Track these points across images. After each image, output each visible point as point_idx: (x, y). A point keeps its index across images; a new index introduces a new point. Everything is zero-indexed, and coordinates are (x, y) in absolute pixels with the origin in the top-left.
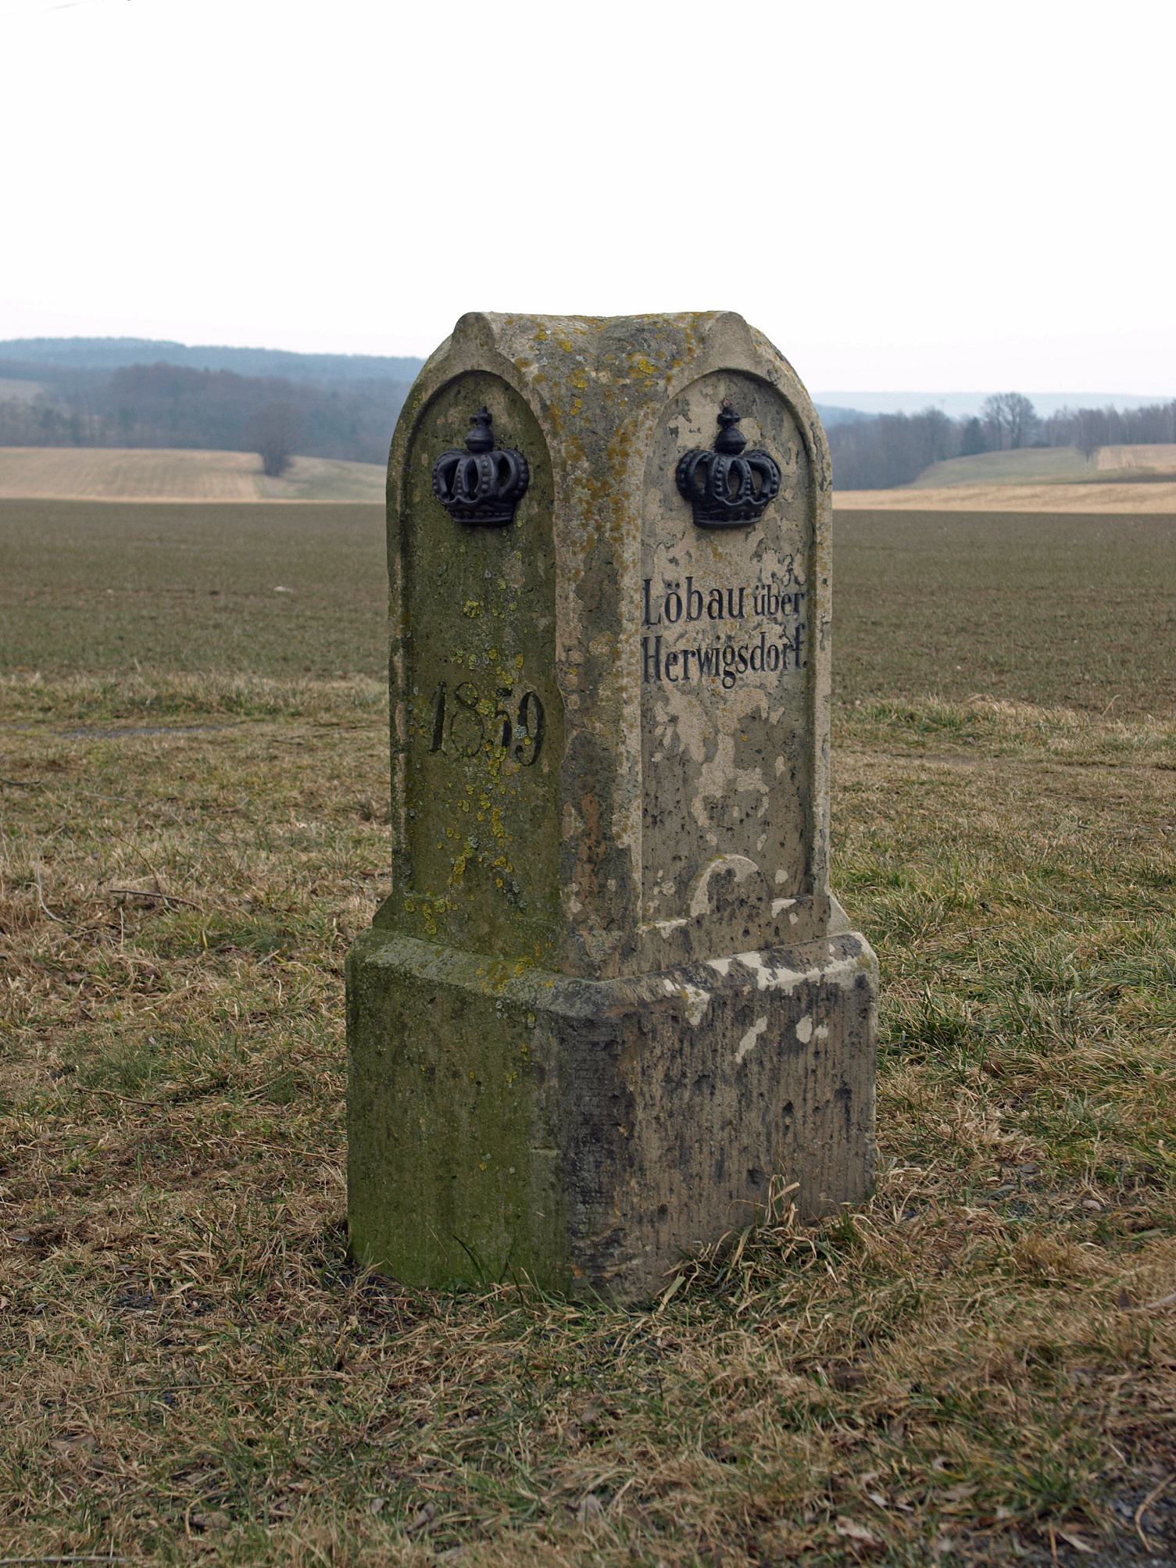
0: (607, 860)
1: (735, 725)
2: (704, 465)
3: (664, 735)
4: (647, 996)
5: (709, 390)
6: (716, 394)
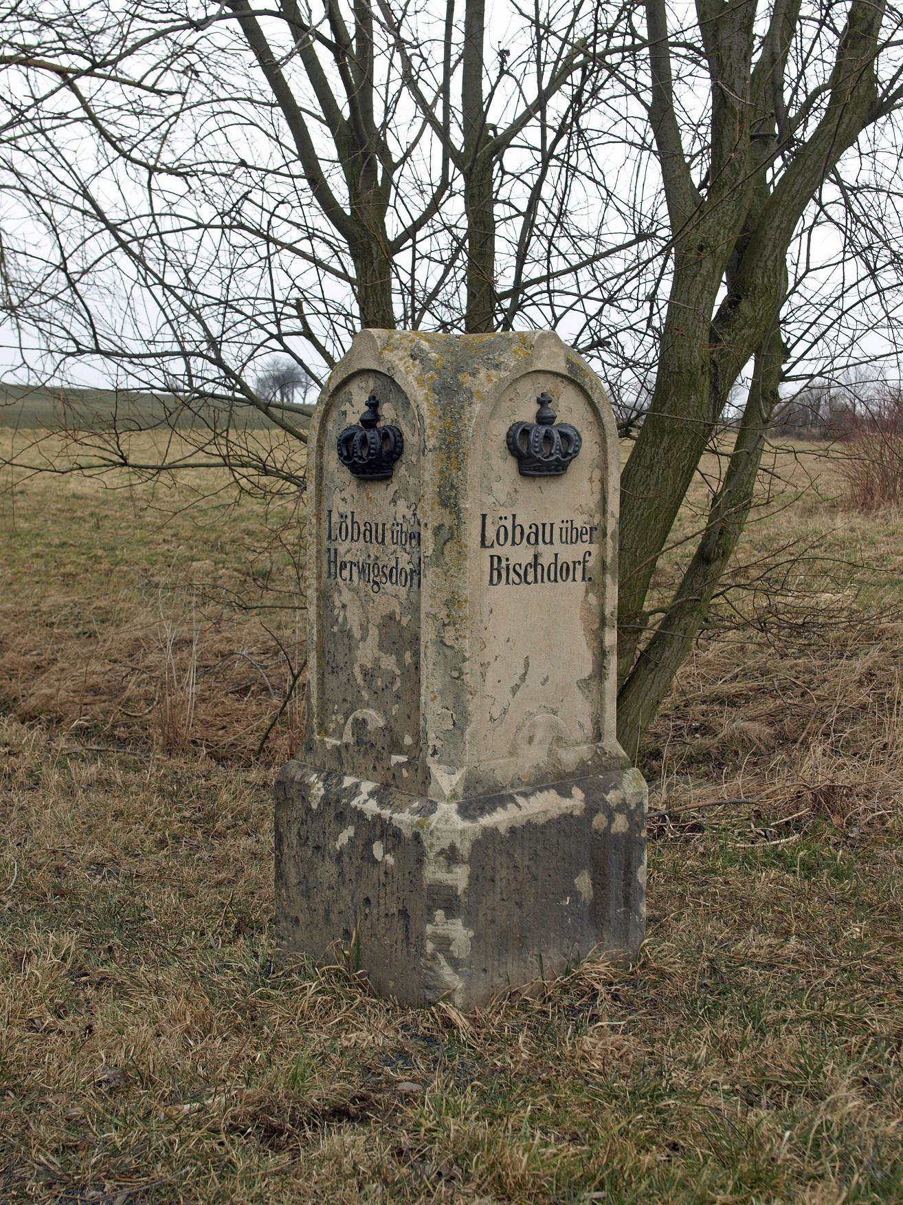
1: (379, 620)
2: (526, 432)
4: (298, 777)
5: (363, 385)
6: (367, 387)
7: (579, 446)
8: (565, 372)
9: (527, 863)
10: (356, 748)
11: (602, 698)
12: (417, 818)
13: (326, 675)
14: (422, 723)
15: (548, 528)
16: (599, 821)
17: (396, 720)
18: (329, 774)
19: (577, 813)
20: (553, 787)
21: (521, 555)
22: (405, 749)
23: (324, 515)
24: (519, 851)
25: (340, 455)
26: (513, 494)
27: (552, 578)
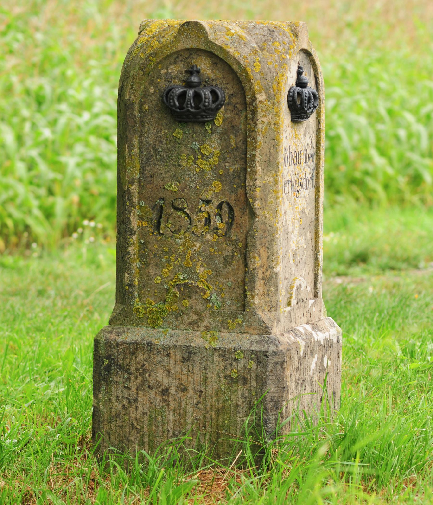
0: (271, 278)
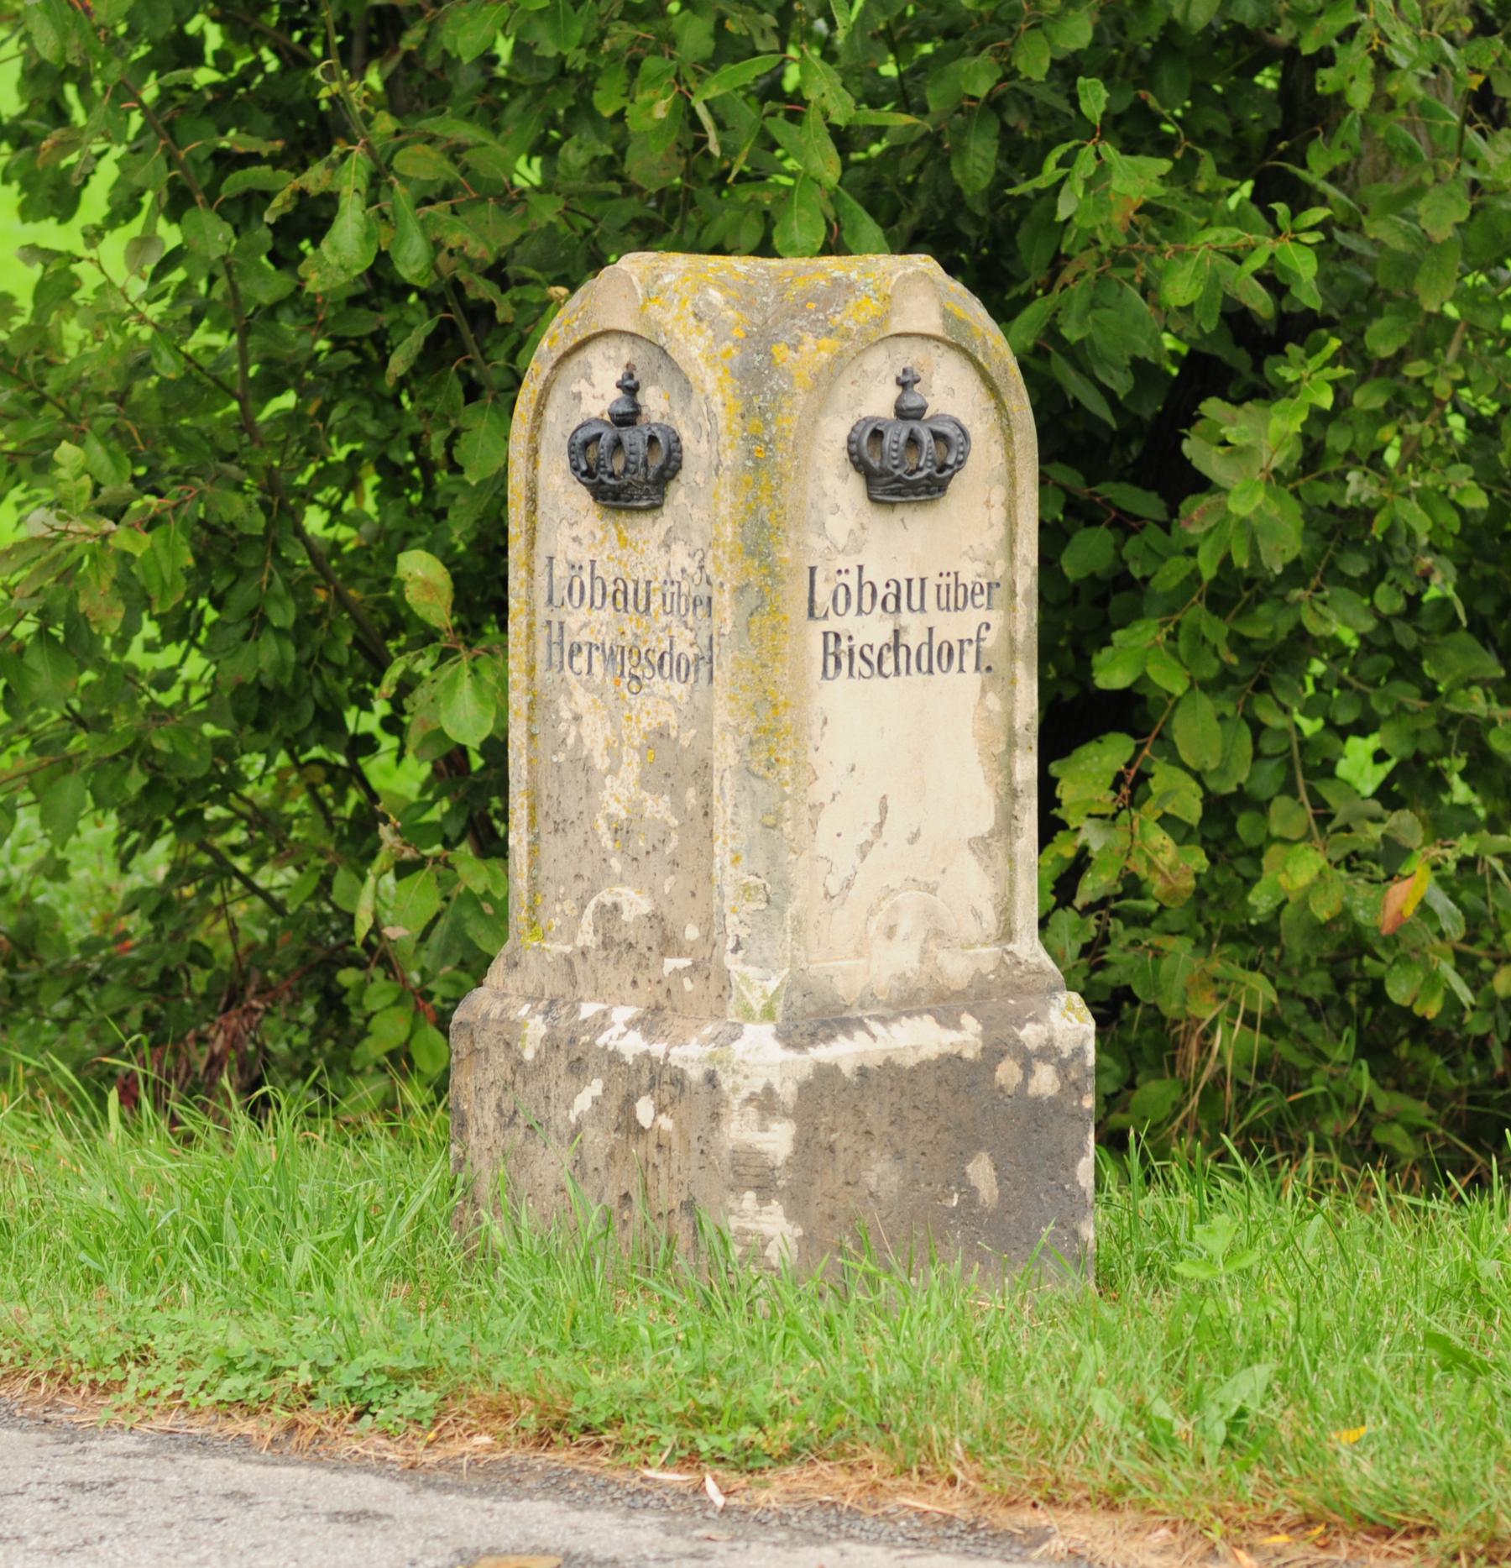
3: (567, 733)
4: (495, 1012)
7: (965, 453)
8: (940, 333)
9: (886, 1128)
10: (602, 954)
11: (1013, 870)
12: (710, 1048)
13: (544, 837)
14: (717, 901)
15: (916, 586)
16: (1007, 1072)
17: (671, 902)
18: (552, 1002)
19: (969, 1054)
20: (929, 1011)
21: (873, 630)
22: (688, 948)
23: (540, 564)
24: (874, 1106)
25: (575, 469)
26: (858, 533)
27: (924, 666)
